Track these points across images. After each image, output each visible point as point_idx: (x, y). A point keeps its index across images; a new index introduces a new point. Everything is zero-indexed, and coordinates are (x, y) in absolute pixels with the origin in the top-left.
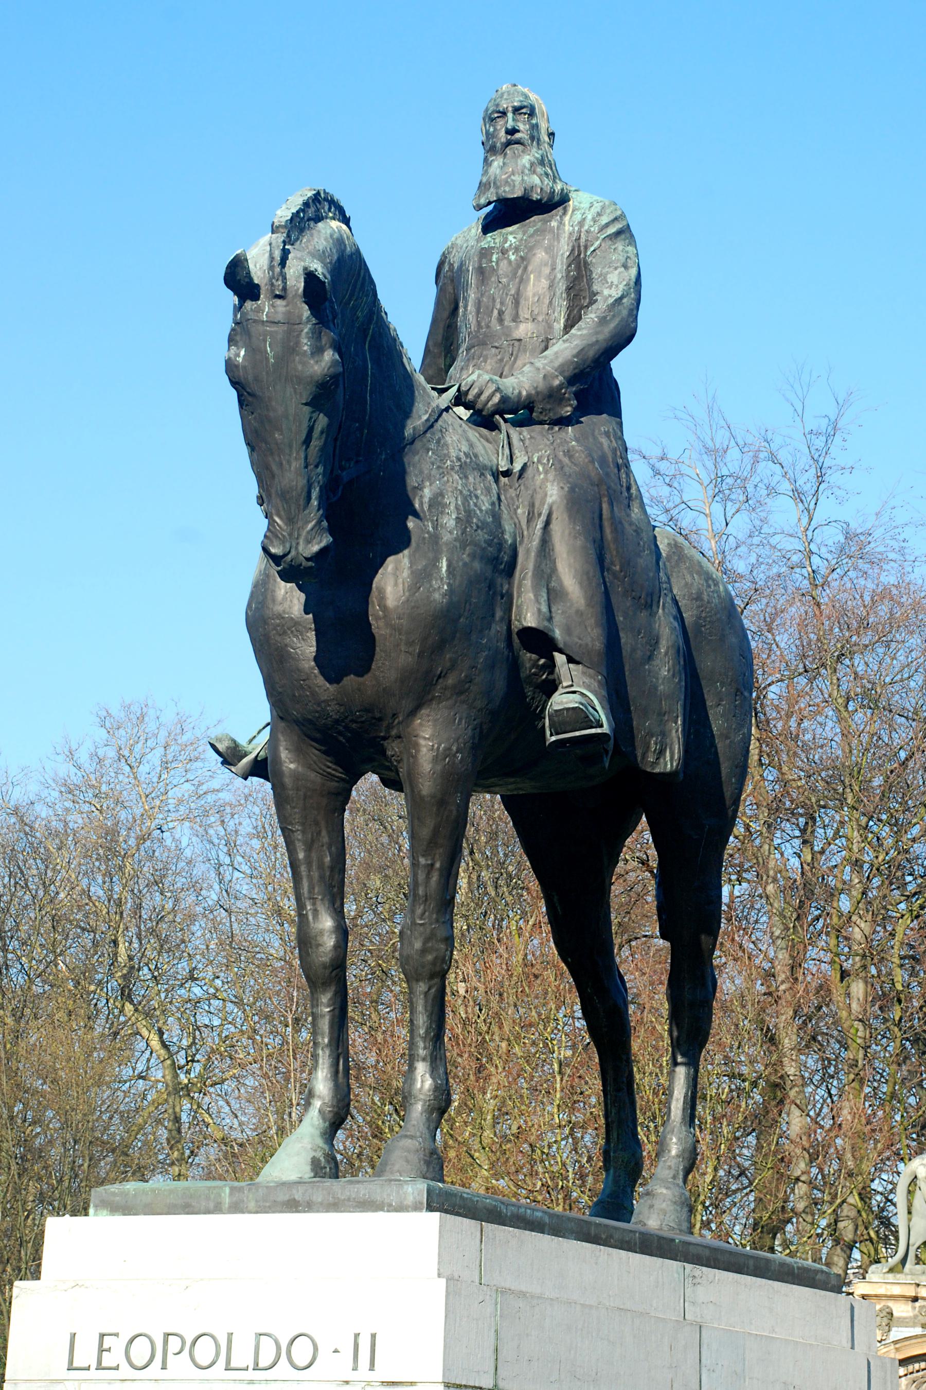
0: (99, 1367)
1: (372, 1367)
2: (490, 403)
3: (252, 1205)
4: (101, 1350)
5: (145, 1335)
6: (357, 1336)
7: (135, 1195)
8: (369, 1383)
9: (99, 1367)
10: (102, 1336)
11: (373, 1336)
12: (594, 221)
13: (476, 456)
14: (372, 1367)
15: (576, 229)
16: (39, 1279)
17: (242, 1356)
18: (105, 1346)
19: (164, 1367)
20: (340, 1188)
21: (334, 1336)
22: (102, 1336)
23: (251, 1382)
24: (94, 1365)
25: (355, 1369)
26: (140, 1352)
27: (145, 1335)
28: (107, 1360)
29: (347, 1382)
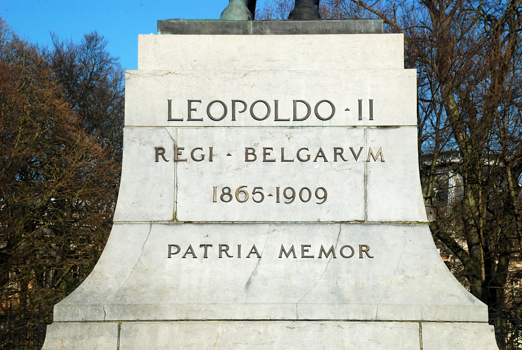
0: (190, 119)
1: (371, 119)
3: (251, 29)
4: (190, 110)
5: (220, 102)
6: (360, 102)
7: (189, 24)
8: (369, 127)
9: (190, 119)
10: (190, 102)
11: (371, 101)
14: (371, 119)
16: (406, 68)
17: (285, 112)
18: (192, 108)
19: (234, 119)
20: (299, 24)
21: (345, 102)
22: (190, 102)
23: (292, 127)
24: (292, 118)
25: (360, 119)
26: (217, 111)
27: (220, 102)
28: (194, 115)
29: (355, 127)
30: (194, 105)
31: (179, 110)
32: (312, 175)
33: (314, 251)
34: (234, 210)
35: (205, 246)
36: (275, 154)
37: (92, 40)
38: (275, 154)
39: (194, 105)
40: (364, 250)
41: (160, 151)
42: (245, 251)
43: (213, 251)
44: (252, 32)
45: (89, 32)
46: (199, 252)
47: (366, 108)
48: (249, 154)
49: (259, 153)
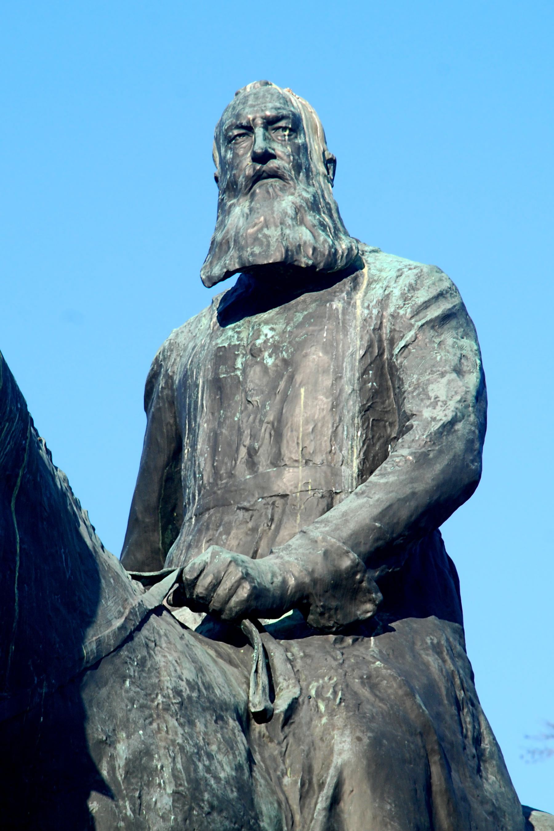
2: (234, 600)
12: (405, 298)
13: (209, 687)
15: (375, 312)
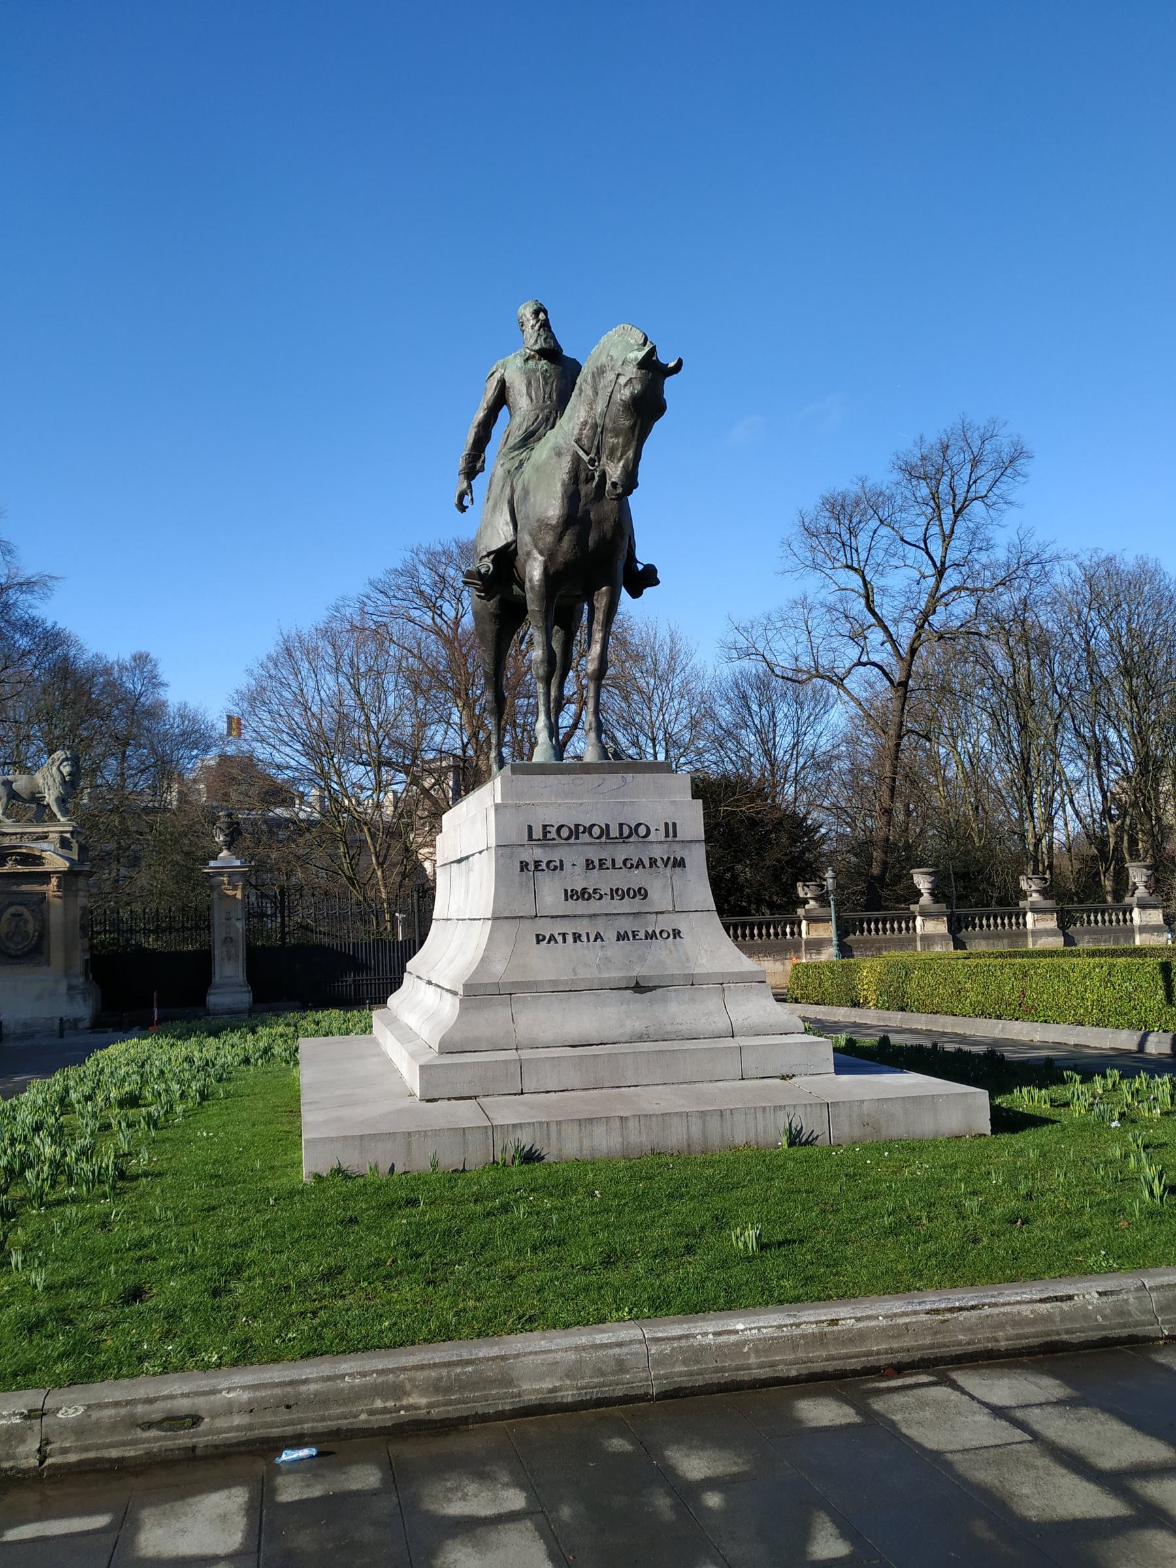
16: (657, 582)
17: (614, 832)
30: (548, 829)
31: (538, 833)
32: (636, 878)
33: (642, 935)
34: (580, 907)
35: (564, 935)
36: (609, 864)
37: (141, 659)
38: (609, 864)
39: (548, 829)
40: (677, 933)
41: (524, 866)
42: (592, 938)
43: (570, 938)
44: (998, 1101)
45: (143, 649)
46: (560, 939)
47: (671, 829)
48: (589, 865)
49: (597, 863)
